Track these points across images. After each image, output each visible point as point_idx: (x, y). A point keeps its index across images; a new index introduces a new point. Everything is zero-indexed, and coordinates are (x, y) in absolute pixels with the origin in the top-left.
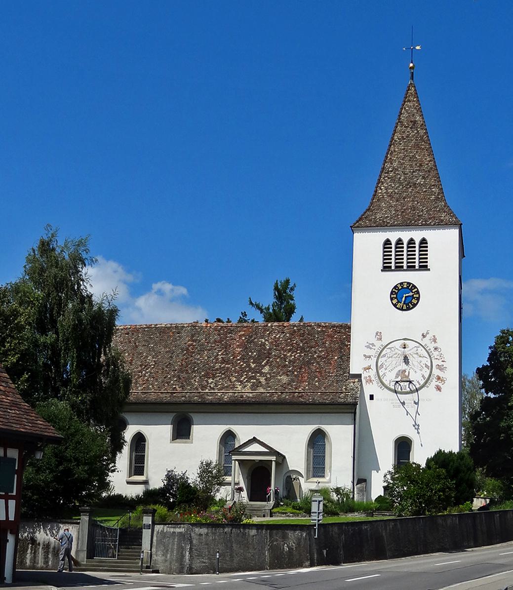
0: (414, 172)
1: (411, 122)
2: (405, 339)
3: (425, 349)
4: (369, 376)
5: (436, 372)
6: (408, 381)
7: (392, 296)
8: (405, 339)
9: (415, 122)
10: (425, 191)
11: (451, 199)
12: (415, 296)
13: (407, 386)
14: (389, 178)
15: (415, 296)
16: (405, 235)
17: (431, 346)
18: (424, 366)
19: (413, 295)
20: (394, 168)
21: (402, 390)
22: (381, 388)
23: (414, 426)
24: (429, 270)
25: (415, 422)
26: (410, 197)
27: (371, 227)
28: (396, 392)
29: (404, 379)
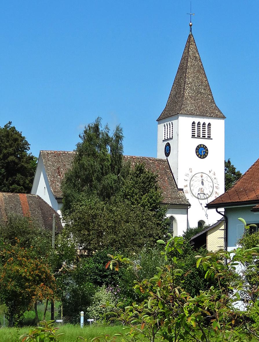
0: (199, 86)
1: (194, 57)
2: (202, 173)
3: (211, 178)
4: (187, 190)
5: (215, 190)
6: (203, 194)
7: (197, 151)
8: (202, 173)
9: (196, 57)
10: (206, 97)
11: (218, 103)
12: (206, 152)
13: (203, 196)
14: (189, 87)
15: (206, 152)
16: (202, 120)
17: (213, 177)
18: (210, 186)
19: (205, 151)
20: (190, 82)
21: (201, 197)
22: (192, 196)
23: (206, 215)
24: (212, 139)
25: (206, 213)
26: (200, 100)
27: (187, 114)
28: (198, 198)
29: (202, 192)
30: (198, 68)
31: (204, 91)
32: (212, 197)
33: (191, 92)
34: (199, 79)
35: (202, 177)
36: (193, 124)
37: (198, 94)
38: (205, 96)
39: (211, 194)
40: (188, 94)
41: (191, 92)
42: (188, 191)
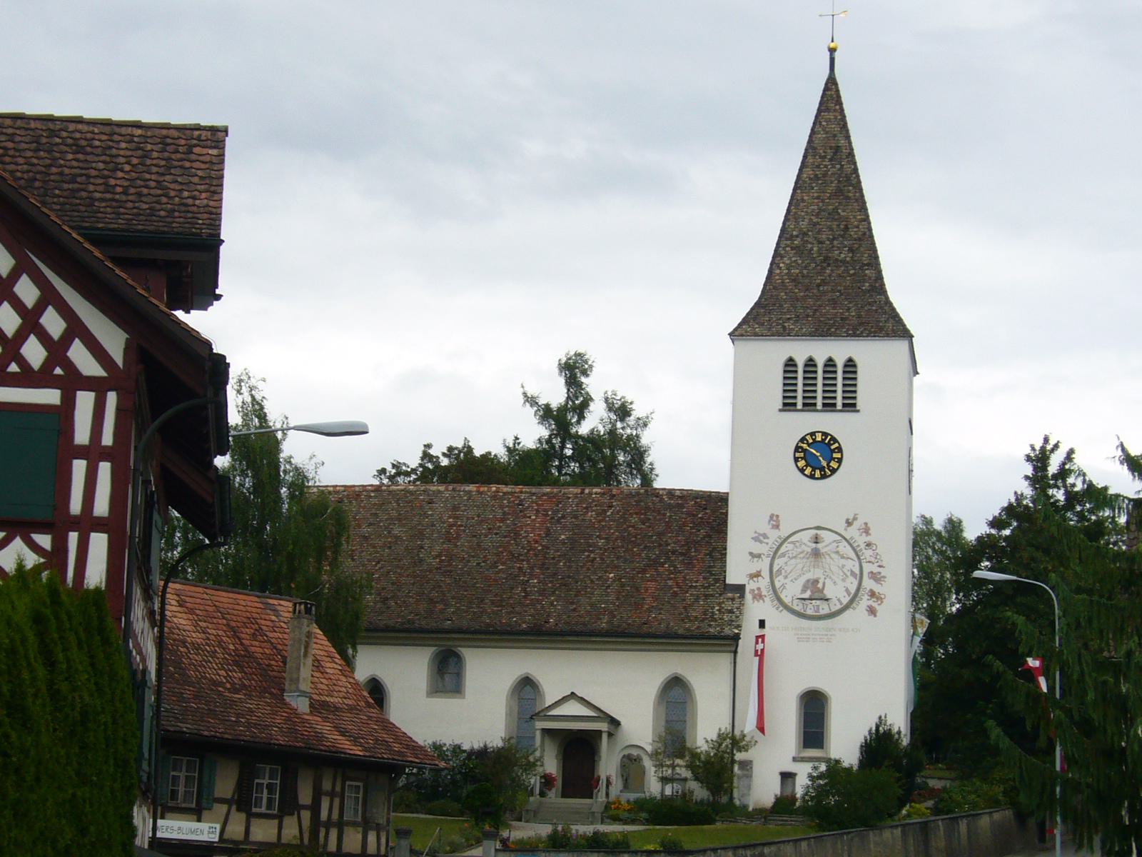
2: (818, 528)
17: (861, 540)
18: (849, 574)
20: (801, 230)
30: (839, 182)
31: (850, 255)
32: (854, 609)
33: (800, 262)
34: (836, 217)
35: (816, 543)
36: (786, 365)
37: (825, 268)
38: (852, 272)
39: (852, 601)
40: (786, 271)
41: (800, 262)
42: (764, 592)
